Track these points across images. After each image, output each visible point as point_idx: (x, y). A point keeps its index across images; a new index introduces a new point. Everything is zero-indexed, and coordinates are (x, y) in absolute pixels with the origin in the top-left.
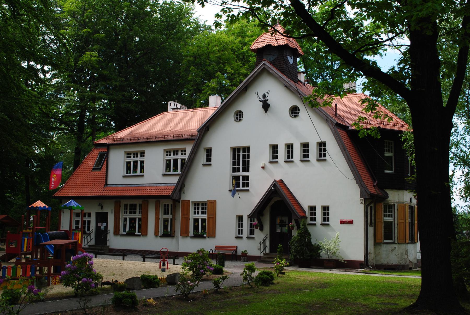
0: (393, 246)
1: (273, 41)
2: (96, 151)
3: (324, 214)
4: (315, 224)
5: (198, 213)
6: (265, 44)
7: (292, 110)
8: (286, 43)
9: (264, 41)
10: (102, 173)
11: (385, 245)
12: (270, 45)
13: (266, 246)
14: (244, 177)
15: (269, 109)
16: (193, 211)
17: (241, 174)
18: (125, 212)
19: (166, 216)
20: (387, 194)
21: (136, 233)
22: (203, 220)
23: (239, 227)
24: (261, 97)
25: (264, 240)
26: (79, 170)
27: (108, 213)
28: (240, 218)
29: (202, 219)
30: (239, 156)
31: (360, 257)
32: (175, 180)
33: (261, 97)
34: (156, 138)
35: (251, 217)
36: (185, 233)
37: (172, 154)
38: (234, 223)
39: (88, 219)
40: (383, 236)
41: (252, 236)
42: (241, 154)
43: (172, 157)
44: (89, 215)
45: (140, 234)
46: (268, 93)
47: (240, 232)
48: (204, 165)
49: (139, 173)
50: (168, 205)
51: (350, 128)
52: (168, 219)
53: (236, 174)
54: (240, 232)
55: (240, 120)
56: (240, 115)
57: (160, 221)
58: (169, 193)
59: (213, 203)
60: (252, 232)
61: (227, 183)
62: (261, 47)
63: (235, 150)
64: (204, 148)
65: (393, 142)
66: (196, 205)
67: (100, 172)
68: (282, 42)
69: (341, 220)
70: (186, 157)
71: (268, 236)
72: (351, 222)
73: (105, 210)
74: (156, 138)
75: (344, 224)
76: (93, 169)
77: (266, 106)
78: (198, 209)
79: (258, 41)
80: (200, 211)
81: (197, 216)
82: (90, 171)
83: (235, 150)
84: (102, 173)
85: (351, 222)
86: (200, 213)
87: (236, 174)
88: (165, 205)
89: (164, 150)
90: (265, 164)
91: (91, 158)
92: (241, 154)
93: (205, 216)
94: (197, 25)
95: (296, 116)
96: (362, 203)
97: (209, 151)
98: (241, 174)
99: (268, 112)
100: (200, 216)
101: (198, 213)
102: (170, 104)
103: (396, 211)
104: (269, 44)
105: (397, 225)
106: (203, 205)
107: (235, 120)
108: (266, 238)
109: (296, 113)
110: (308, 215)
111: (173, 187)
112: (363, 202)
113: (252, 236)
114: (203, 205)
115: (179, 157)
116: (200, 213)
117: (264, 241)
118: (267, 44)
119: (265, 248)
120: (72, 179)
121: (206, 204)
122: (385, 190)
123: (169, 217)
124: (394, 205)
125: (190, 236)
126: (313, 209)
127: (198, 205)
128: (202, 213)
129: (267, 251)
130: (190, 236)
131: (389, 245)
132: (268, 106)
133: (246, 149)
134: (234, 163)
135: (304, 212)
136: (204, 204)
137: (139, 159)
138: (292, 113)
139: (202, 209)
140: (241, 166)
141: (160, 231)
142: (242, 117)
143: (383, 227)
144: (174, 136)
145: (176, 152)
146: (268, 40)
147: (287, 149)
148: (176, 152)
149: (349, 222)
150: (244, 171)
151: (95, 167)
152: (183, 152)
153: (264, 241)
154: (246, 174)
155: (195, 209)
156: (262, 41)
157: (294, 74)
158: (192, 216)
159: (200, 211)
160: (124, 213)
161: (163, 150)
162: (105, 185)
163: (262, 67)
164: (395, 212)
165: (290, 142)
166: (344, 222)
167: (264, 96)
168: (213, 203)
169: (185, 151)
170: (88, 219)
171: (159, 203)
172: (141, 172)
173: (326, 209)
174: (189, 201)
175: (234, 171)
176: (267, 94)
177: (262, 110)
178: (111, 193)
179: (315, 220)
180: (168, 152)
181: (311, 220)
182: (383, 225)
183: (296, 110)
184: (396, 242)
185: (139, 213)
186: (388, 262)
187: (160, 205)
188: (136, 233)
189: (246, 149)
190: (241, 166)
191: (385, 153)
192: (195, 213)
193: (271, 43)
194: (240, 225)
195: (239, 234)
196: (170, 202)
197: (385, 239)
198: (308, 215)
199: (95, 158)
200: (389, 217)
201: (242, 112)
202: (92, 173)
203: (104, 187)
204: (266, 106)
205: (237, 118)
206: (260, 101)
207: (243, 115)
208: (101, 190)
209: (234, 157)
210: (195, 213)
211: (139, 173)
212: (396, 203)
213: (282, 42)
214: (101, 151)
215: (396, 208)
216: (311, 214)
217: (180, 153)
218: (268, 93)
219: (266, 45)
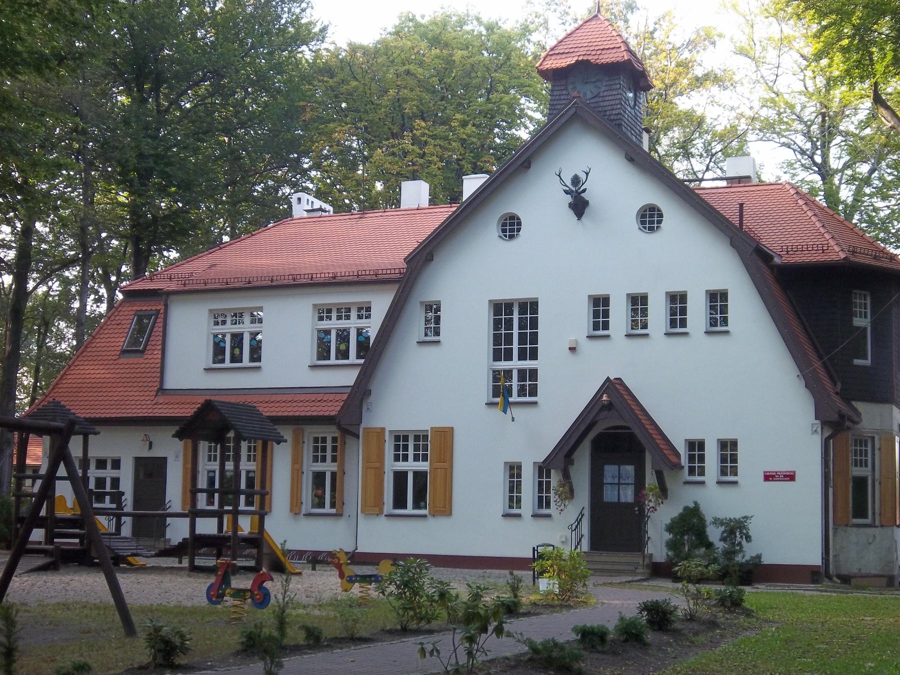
0: (870, 531)
1: (593, 53)
2: (124, 309)
3: (723, 459)
4: (702, 483)
5: (406, 458)
6: (576, 59)
7: (643, 216)
8: (626, 58)
9: (571, 50)
10: (146, 361)
11: (855, 529)
12: (588, 61)
13: (582, 536)
14: (522, 373)
15: (586, 211)
16: (393, 453)
17: (515, 364)
18: (210, 456)
19: (319, 467)
20: (858, 414)
21: (240, 508)
22: (420, 477)
23: (511, 491)
24: (569, 183)
25: (579, 521)
26: (84, 354)
27: (165, 459)
28: (514, 470)
29: (417, 474)
30: (509, 324)
31: (814, 558)
32: (348, 378)
33: (569, 183)
34: (205, 284)
35: (543, 469)
36: (373, 507)
37: (334, 315)
38: (499, 481)
39: (114, 473)
40: (851, 509)
41: (515, 511)
42: (516, 317)
43: (334, 324)
44: (116, 464)
45: (334, 511)
46: (587, 174)
47: (514, 500)
48: (420, 343)
49: (246, 362)
50: (324, 440)
51: (777, 260)
52: (105, 479)
53: (503, 365)
54: (514, 500)
55: (511, 237)
56: (512, 224)
57: (304, 476)
58: (332, 410)
59: (445, 436)
60: (543, 502)
61: (483, 387)
62: (563, 65)
63: (501, 309)
64: (421, 303)
65: (868, 293)
66: (401, 439)
67: (142, 361)
68: (616, 55)
69: (765, 472)
70: (373, 327)
71: (587, 513)
72: (790, 477)
73: (157, 453)
74: (205, 284)
75: (773, 480)
76: (124, 352)
77: (579, 206)
78: (406, 448)
79: (556, 52)
80: (411, 453)
81: (401, 466)
82: (114, 358)
83: (501, 309)
84: (146, 361)
85: (790, 477)
86: (411, 457)
87: (503, 365)
88: (316, 440)
89: (315, 306)
90: (576, 341)
91: (115, 327)
92: (516, 317)
93: (423, 466)
94: (214, 25)
95: (651, 229)
96: (816, 431)
97: (433, 308)
98: (515, 364)
99: (584, 218)
100: (411, 466)
101: (406, 458)
102: (299, 199)
103: (877, 452)
104: (585, 58)
105: (880, 483)
106: (417, 438)
107: (500, 237)
108: (582, 516)
109: (512, 230)
110: (684, 461)
111: (345, 397)
112: (819, 430)
113: (515, 511)
114: (417, 438)
115: (353, 324)
116: (411, 457)
117: (578, 523)
118: (580, 58)
119: (580, 540)
120: (69, 377)
121: (425, 437)
122: (854, 403)
123: (328, 467)
124: (873, 438)
125: (385, 513)
126: (696, 447)
127: (406, 438)
128: (416, 458)
129: (585, 546)
130: (385, 513)
131: (862, 530)
132: (585, 204)
133: (530, 307)
134: (497, 339)
135: (678, 455)
136: (420, 437)
137: (246, 327)
138: (643, 223)
139: (416, 448)
140: (515, 346)
141: (304, 502)
142: (519, 230)
143: (851, 489)
144: (314, 276)
145: (344, 312)
146: (581, 49)
147: (592, 309)
148: (344, 312)
149: (785, 476)
150: (522, 357)
151: (127, 347)
152: (365, 311)
153: (578, 523)
154: (528, 364)
155: (397, 448)
156: (566, 51)
157: (637, 131)
158: (391, 466)
159: (411, 453)
160: (210, 460)
161: (311, 308)
162: (158, 391)
163: (574, 110)
164: (873, 454)
165: (599, 291)
166: (773, 476)
167: (576, 180)
168: (445, 436)
169: (369, 309)
170: (114, 473)
171: (303, 436)
172: (252, 359)
173: (728, 449)
174: (383, 429)
175: (497, 357)
176: (583, 176)
177: (571, 214)
178: (177, 411)
179: (702, 473)
180: (324, 313)
181: (692, 471)
182: (851, 485)
183: (512, 224)
184: (877, 523)
185: (249, 460)
186: (860, 570)
187: (306, 441)
188: (240, 508)
189: (530, 307)
190: (515, 346)
191: (855, 319)
192: (397, 458)
193: (590, 58)
194: (514, 486)
195: (511, 507)
196: (329, 432)
197: (854, 517)
198: (684, 461)
199: (124, 327)
200: (861, 466)
201: (518, 219)
202: (121, 361)
203: (156, 396)
204: (579, 206)
205: (504, 231)
206: (566, 192)
207: (519, 224)
208: (149, 402)
209: (497, 324)
210: (397, 458)
211: (246, 362)
212: (877, 433)
213: (616, 55)
214: (139, 309)
215: (877, 445)
216: (691, 458)
217: (354, 314)
218: (587, 174)
219: (577, 61)
